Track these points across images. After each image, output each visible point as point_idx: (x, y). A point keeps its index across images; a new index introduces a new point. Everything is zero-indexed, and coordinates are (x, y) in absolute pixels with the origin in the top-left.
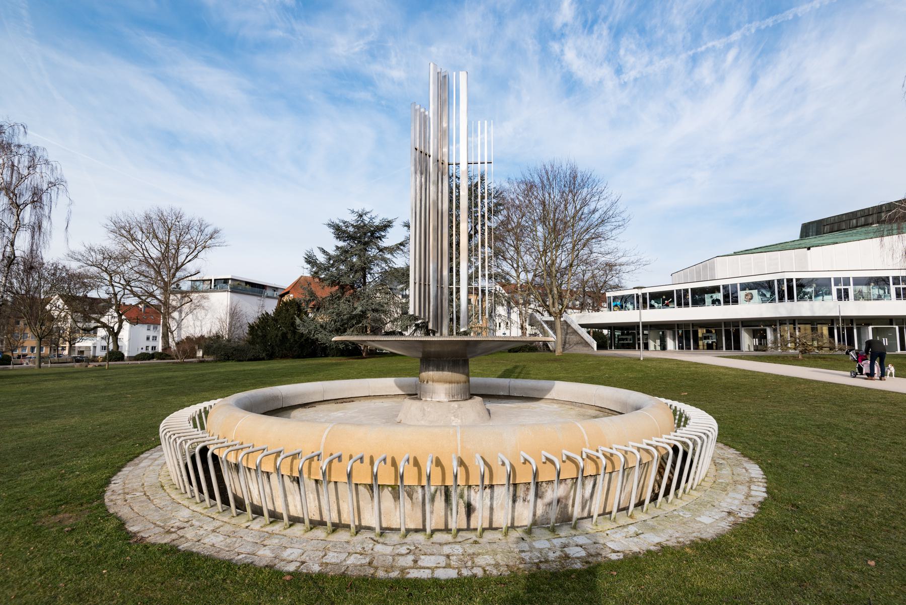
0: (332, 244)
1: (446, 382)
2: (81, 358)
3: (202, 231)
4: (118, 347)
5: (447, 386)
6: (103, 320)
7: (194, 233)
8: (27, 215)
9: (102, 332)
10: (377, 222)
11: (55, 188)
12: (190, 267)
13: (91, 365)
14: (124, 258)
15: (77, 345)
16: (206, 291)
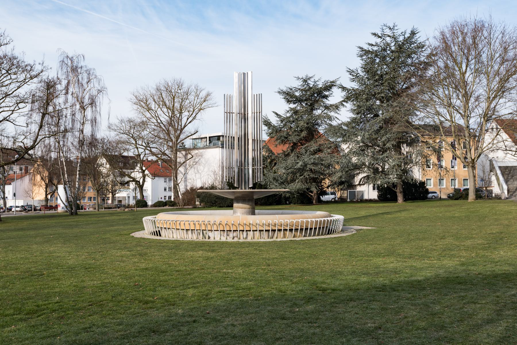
0: (284, 108)
1: (240, 208)
2: (120, 204)
3: (198, 96)
4: (143, 196)
5: (240, 209)
6: (133, 175)
7: (191, 97)
8: (89, 113)
9: (132, 185)
10: (320, 85)
11: (101, 93)
12: (190, 129)
13: (127, 210)
14: (144, 124)
15: (117, 195)
16: (203, 148)
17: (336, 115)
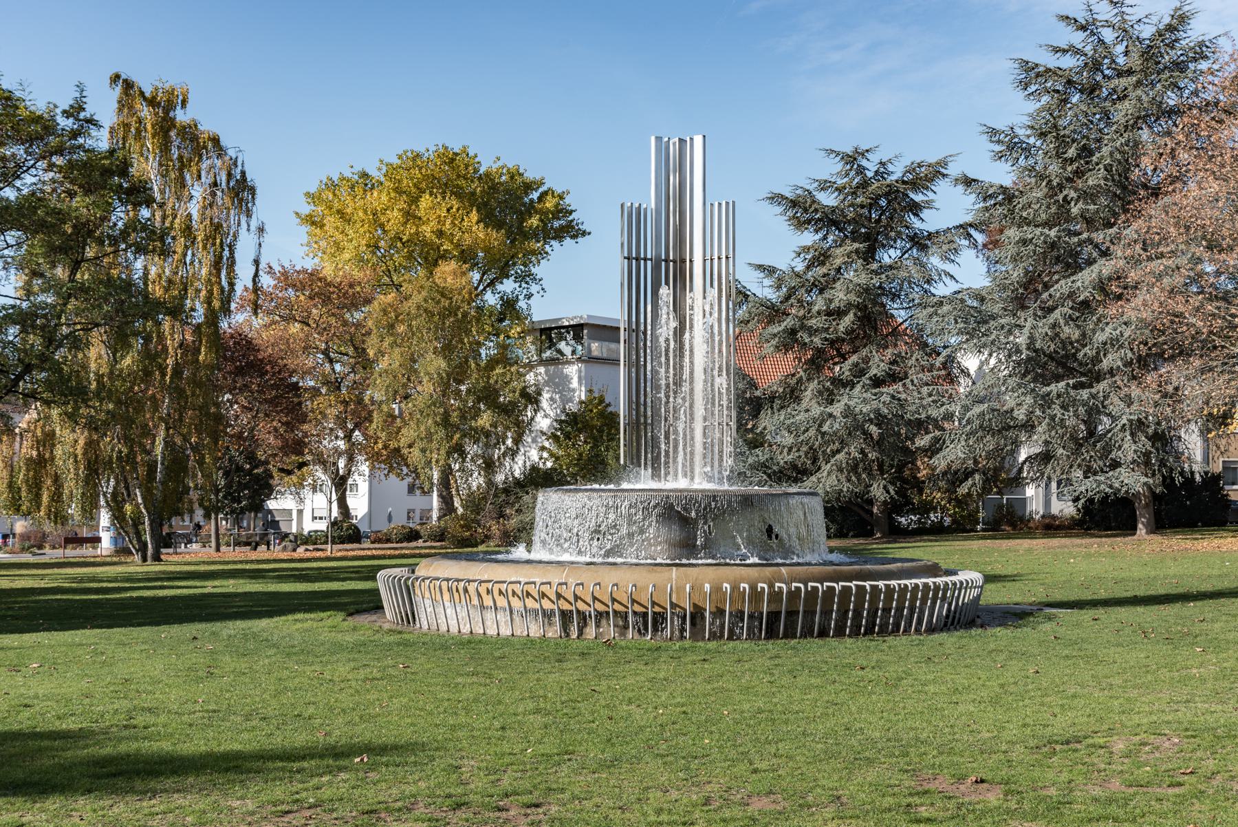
0: (786, 246)
10: (897, 172)
17: (948, 267)
